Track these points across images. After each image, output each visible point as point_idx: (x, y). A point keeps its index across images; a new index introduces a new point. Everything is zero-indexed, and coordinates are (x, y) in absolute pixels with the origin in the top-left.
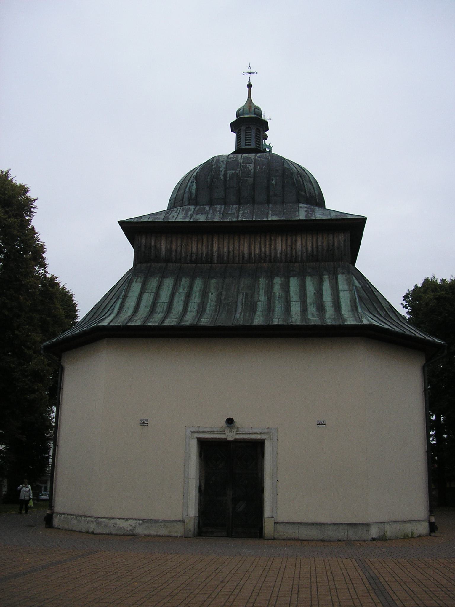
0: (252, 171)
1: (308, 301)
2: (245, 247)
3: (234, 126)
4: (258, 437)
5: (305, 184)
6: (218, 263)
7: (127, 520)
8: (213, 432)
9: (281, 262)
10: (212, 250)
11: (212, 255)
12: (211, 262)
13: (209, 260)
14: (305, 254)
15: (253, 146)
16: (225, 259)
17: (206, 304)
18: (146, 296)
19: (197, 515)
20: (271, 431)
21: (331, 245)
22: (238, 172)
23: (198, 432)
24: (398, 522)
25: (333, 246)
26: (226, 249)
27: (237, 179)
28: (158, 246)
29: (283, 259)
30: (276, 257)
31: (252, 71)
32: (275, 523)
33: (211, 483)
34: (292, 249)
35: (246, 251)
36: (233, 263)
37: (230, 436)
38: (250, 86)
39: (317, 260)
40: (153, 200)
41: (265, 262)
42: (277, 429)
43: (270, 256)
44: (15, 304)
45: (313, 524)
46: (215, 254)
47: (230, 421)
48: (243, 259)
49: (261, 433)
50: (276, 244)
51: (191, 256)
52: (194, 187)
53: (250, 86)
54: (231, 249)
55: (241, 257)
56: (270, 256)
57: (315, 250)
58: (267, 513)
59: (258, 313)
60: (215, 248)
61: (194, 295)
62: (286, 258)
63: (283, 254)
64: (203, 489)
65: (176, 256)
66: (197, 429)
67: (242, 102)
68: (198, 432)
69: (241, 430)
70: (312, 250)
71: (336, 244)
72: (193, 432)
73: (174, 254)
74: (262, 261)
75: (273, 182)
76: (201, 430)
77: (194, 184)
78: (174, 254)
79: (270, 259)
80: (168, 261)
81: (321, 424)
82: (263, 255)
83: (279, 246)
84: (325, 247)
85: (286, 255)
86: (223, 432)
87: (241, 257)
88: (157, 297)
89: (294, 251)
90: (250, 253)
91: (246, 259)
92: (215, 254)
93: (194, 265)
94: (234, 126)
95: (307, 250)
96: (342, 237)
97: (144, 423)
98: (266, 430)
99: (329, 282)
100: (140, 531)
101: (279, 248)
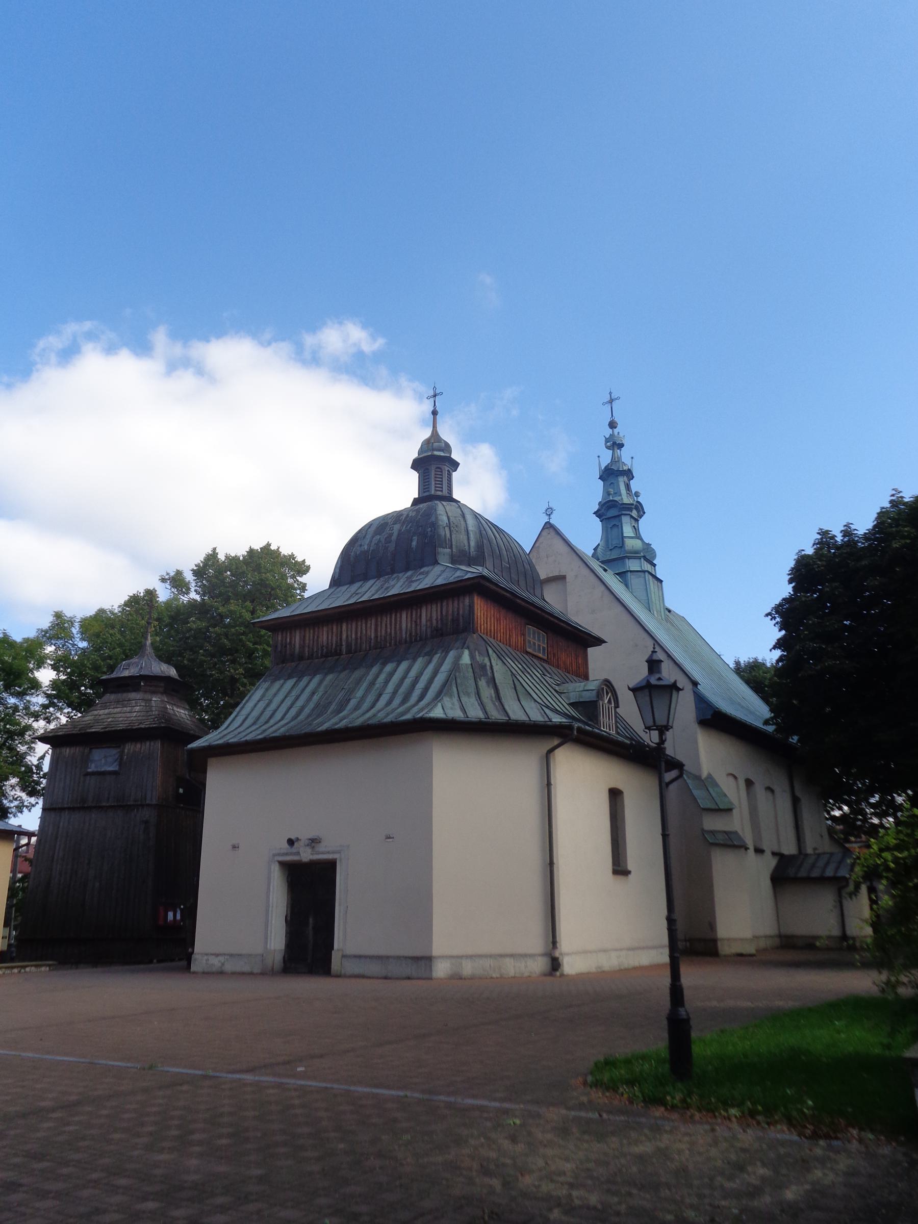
2: (369, 629)
3: (417, 465)
4: (330, 857)
5: (453, 536)
7: (217, 955)
10: (341, 639)
11: (341, 645)
12: (340, 654)
14: (429, 630)
18: (261, 703)
24: (491, 956)
25: (458, 614)
31: (438, 392)
34: (416, 625)
37: (306, 855)
40: (596, 508)
43: (395, 637)
44: (784, 1171)
46: (344, 643)
47: (291, 842)
49: (333, 853)
51: (322, 650)
54: (359, 634)
56: (395, 637)
58: (336, 946)
60: (344, 636)
62: (411, 638)
67: (427, 434)
68: (279, 855)
71: (461, 612)
72: (274, 855)
73: (307, 649)
78: (307, 649)
79: (396, 642)
80: (301, 658)
83: (404, 620)
84: (450, 618)
88: (270, 702)
90: (376, 637)
94: (417, 465)
95: (432, 624)
97: (235, 847)
100: (228, 967)
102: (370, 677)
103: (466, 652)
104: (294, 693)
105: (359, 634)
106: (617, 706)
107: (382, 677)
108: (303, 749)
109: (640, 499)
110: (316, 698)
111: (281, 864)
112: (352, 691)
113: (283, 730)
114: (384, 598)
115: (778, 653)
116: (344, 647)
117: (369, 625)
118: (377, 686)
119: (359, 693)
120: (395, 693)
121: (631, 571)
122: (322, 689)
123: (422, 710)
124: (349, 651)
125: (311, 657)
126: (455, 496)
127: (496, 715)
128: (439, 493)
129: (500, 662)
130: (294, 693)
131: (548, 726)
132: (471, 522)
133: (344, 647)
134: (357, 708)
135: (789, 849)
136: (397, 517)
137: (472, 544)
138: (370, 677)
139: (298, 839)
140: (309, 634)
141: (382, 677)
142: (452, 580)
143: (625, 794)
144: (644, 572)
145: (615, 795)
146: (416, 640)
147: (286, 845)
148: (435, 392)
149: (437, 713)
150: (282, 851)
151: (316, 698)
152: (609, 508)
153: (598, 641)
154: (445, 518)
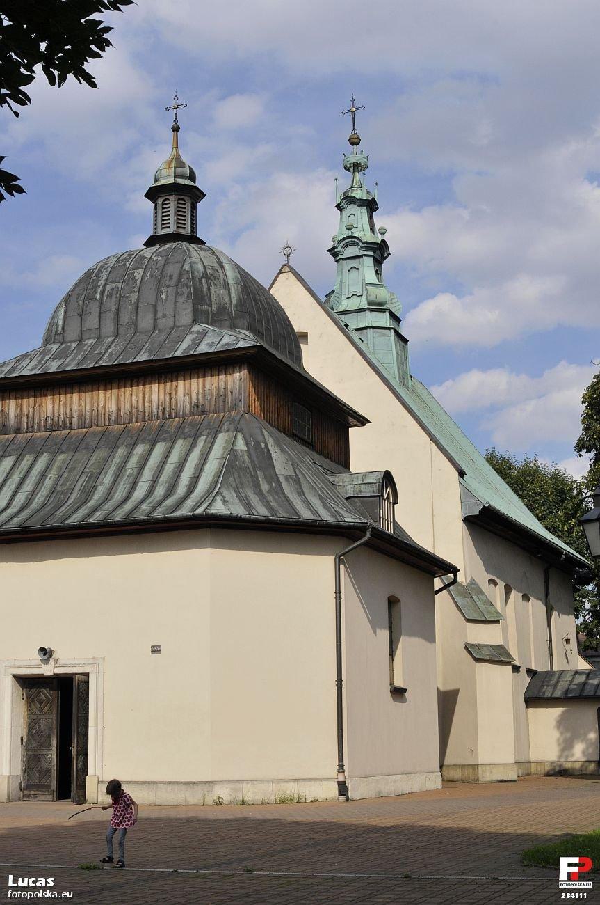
0: (138, 282)
1: (161, 479)
2: (106, 402)
4: (81, 670)
6: (78, 428)
8: (30, 667)
9: (158, 419)
10: (71, 410)
12: (70, 428)
13: (68, 425)
15: (172, 229)
16: (88, 421)
17: (38, 493)
19: (18, 771)
20: (97, 662)
21: (223, 387)
22: (119, 285)
23: (14, 667)
24: (273, 781)
26: (88, 407)
27: (116, 297)
28: (6, 410)
29: (160, 414)
30: (151, 413)
31: (180, 102)
32: (98, 782)
33: (34, 731)
35: (114, 409)
36: (97, 426)
37: (48, 670)
38: (176, 129)
39: (204, 412)
41: (137, 421)
42: (104, 659)
45: (143, 783)
46: (75, 415)
47: (46, 653)
48: (110, 419)
50: (151, 394)
52: (62, 316)
53: (176, 129)
55: (107, 415)
57: (201, 399)
58: (91, 770)
59: (261, 482)
60: (75, 407)
61: (28, 482)
63: (160, 408)
64: (25, 740)
65: (27, 423)
66: (12, 664)
69: (60, 662)
70: (198, 399)
71: (229, 387)
73: (24, 419)
74: (134, 420)
75: (163, 296)
76: (17, 663)
77: (62, 311)
78: (24, 419)
81: (156, 650)
82: (134, 410)
83: (154, 395)
85: (64, 421)
86: (38, 666)
87: (107, 415)
89: (173, 401)
90: (119, 409)
91: (113, 418)
92: (75, 415)
93: (49, 433)
96: (237, 375)
98: (91, 661)
99: (203, 447)
101: (155, 398)
102: (117, 460)
103: (240, 437)
104: (17, 476)
105: (95, 406)
106: (395, 502)
107: (134, 461)
108: (35, 543)
109: (385, 237)
110: (48, 482)
111: (15, 677)
112: (95, 478)
113: (16, 520)
114: (113, 366)
115: (588, 458)
116: (75, 421)
117: (108, 395)
118: (129, 471)
119: (108, 479)
120: (155, 481)
121: (374, 328)
122: (53, 474)
123: (199, 505)
124: (82, 426)
125: (31, 428)
126: (200, 235)
127: (283, 515)
128: (182, 231)
129: (278, 450)
130: (17, 476)
131: (275, 522)
132: (231, 274)
133: (75, 421)
134: (107, 498)
135: (542, 667)
136: (292, 328)
137: (234, 301)
138: (117, 460)
139: (51, 651)
140: (27, 404)
141: (134, 461)
142: (219, 348)
143: (402, 603)
144: (389, 329)
145: (393, 602)
146: (170, 416)
147: (37, 657)
148: (176, 103)
149: (219, 508)
150: (33, 663)
151: (48, 482)
152: (348, 245)
153: (363, 421)
154: (201, 268)
